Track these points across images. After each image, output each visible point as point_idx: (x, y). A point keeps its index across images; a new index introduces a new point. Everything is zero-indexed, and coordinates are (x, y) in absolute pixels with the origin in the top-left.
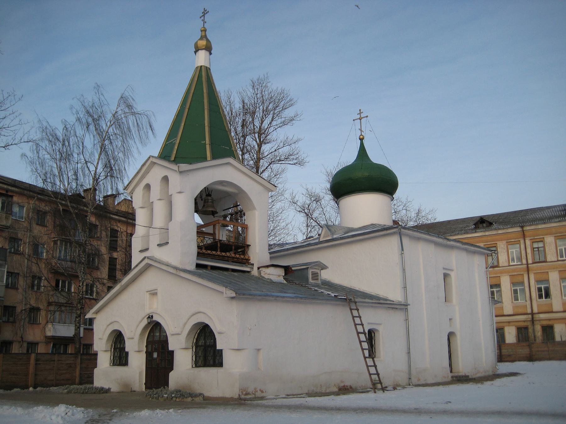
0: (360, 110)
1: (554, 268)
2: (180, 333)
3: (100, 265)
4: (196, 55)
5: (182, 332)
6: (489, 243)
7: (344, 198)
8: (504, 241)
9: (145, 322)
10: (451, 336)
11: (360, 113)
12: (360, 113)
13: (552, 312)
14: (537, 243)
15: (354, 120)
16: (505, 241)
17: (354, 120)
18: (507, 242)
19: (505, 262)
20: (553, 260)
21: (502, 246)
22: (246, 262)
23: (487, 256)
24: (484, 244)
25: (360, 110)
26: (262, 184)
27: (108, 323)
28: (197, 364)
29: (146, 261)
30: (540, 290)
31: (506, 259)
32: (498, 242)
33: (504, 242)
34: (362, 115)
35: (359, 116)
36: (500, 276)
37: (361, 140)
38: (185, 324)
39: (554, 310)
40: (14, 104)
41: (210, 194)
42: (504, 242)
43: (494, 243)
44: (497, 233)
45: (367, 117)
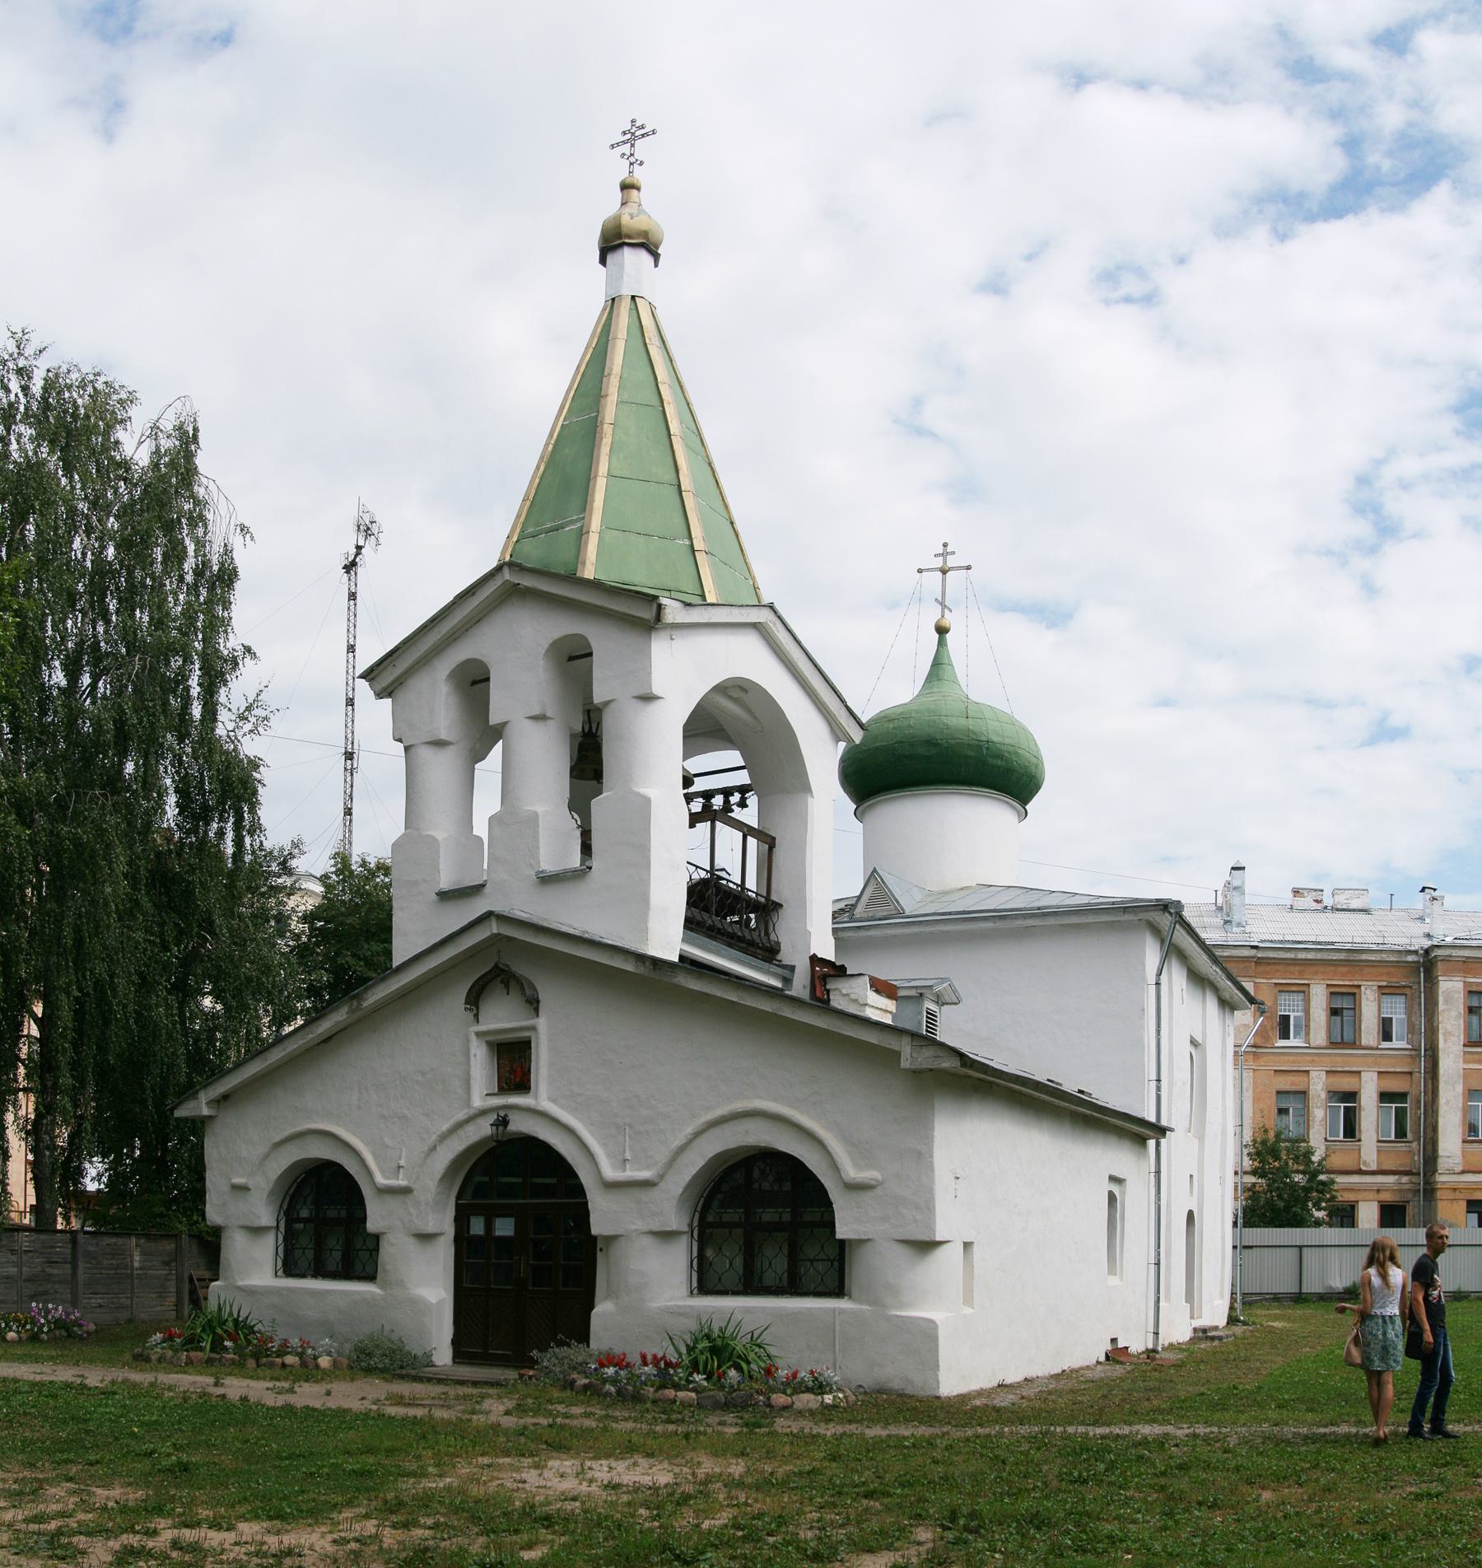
0: (945, 545)
2: (655, 1180)
5: (662, 1176)
7: (880, 801)
9: (484, 1129)
10: (1190, 1215)
11: (944, 555)
12: (944, 555)
15: (920, 571)
17: (920, 571)
22: (768, 953)
25: (945, 545)
27: (277, 1139)
29: (494, 928)
34: (951, 562)
35: (939, 562)
37: (942, 631)
38: (681, 1150)
41: (594, 731)
45: (968, 568)
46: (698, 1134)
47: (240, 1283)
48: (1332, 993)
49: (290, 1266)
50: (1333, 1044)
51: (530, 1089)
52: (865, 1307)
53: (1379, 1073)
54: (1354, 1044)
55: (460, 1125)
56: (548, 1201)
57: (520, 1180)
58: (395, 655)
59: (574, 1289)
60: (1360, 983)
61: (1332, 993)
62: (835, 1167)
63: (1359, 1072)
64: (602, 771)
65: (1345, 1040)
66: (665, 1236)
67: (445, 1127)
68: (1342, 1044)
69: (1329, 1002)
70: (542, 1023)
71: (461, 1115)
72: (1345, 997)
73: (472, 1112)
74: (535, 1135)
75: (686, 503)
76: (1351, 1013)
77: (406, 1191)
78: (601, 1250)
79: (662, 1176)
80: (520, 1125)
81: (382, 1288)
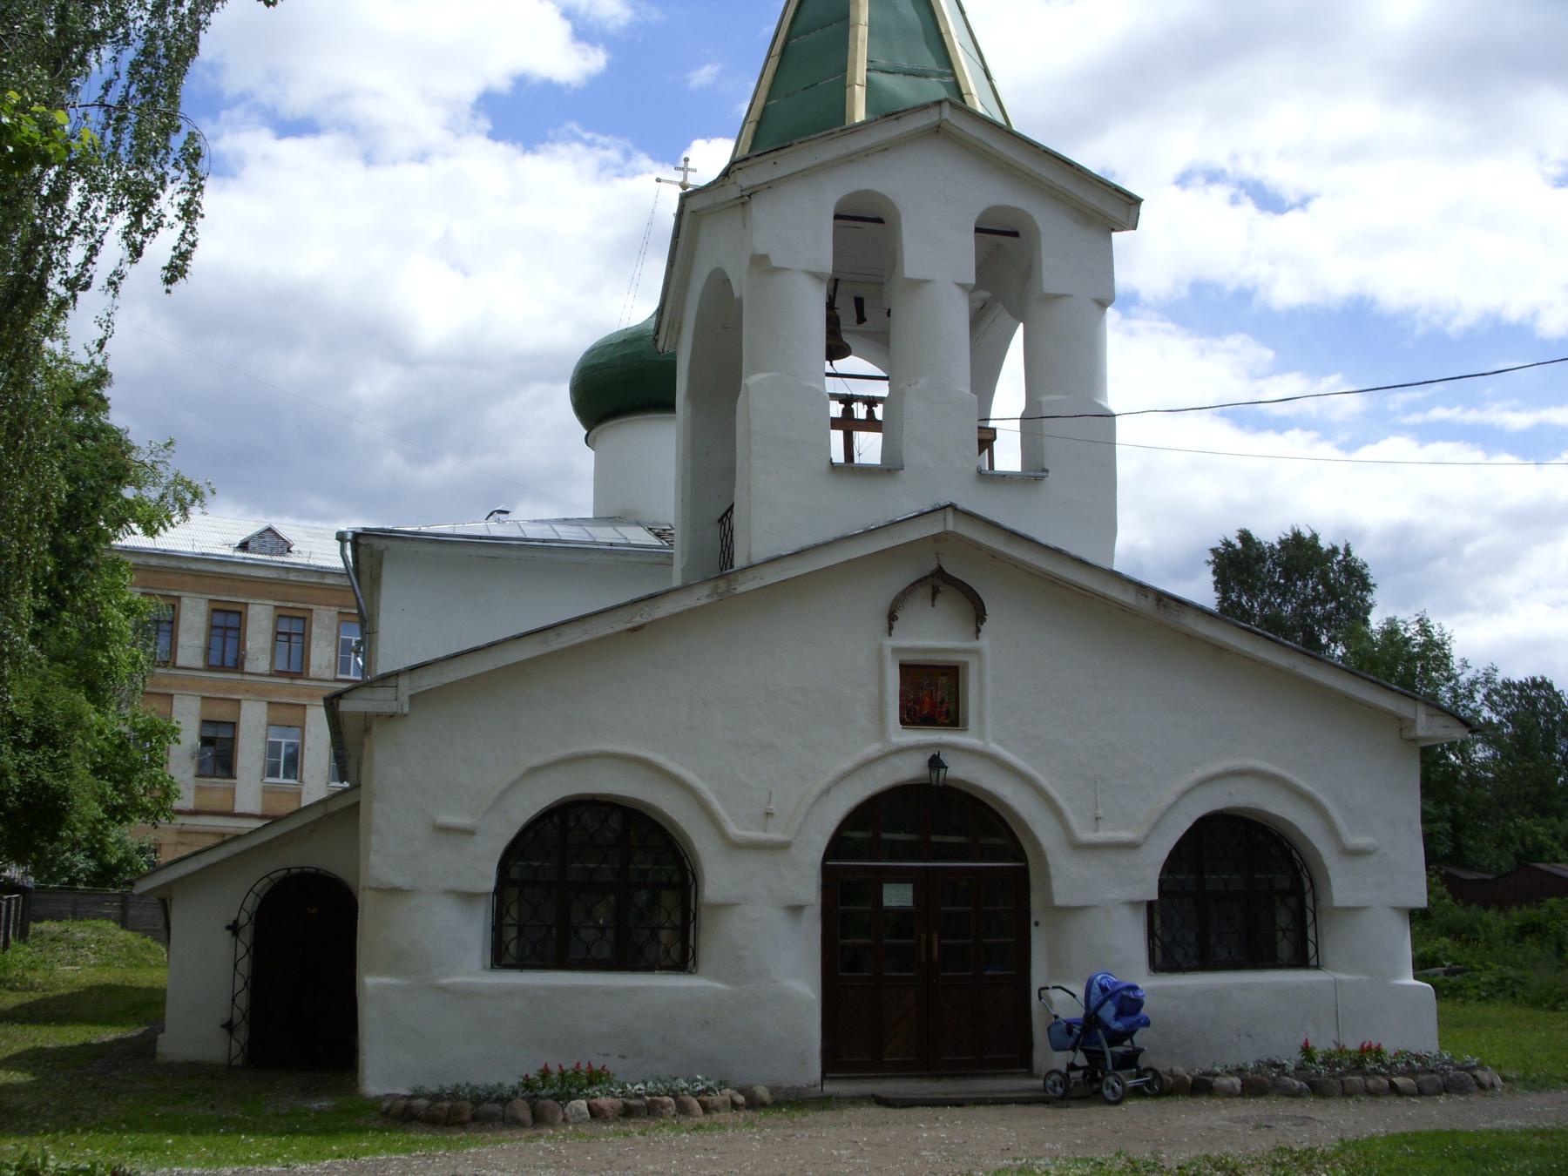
1: (258, 693)
3: (158, 81)
4: (958, 284)
6: (291, 605)
8: (333, 608)
13: (231, 814)
14: (288, 620)
16: (337, 608)
18: (340, 613)
19: (326, 667)
20: (260, 670)
21: (327, 620)
23: (165, 664)
24: (277, 604)
26: (679, 230)
28: (500, 958)
30: (273, 749)
31: (330, 661)
32: (316, 607)
33: (334, 611)
36: (305, 706)
39: (238, 809)
40: (604, 1055)
42: (334, 611)
43: (304, 606)
44: (320, 581)
46: (1186, 792)
47: (444, 981)
48: (214, 610)
49: (500, 958)
50: (210, 667)
51: (966, 723)
52: (1362, 977)
53: (203, 698)
54: (238, 666)
55: (868, 764)
56: (891, 864)
57: (884, 836)
58: (907, 112)
59: (894, 974)
60: (310, 607)
61: (214, 610)
62: (1333, 831)
63: (172, 695)
64: (827, 308)
65: (226, 664)
66: (468, 897)
67: (846, 764)
68: (222, 668)
69: (276, 624)
70: (984, 642)
71: (873, 749)
72: (294, 621)
73: (888, 748)
74: (977, 783)
75: (958, 9)
76: (234, 633)
77: (783, 847)
78: (1037, 924)
79: (1146, 838)
80: (959, 770)
81: (716, 976)
